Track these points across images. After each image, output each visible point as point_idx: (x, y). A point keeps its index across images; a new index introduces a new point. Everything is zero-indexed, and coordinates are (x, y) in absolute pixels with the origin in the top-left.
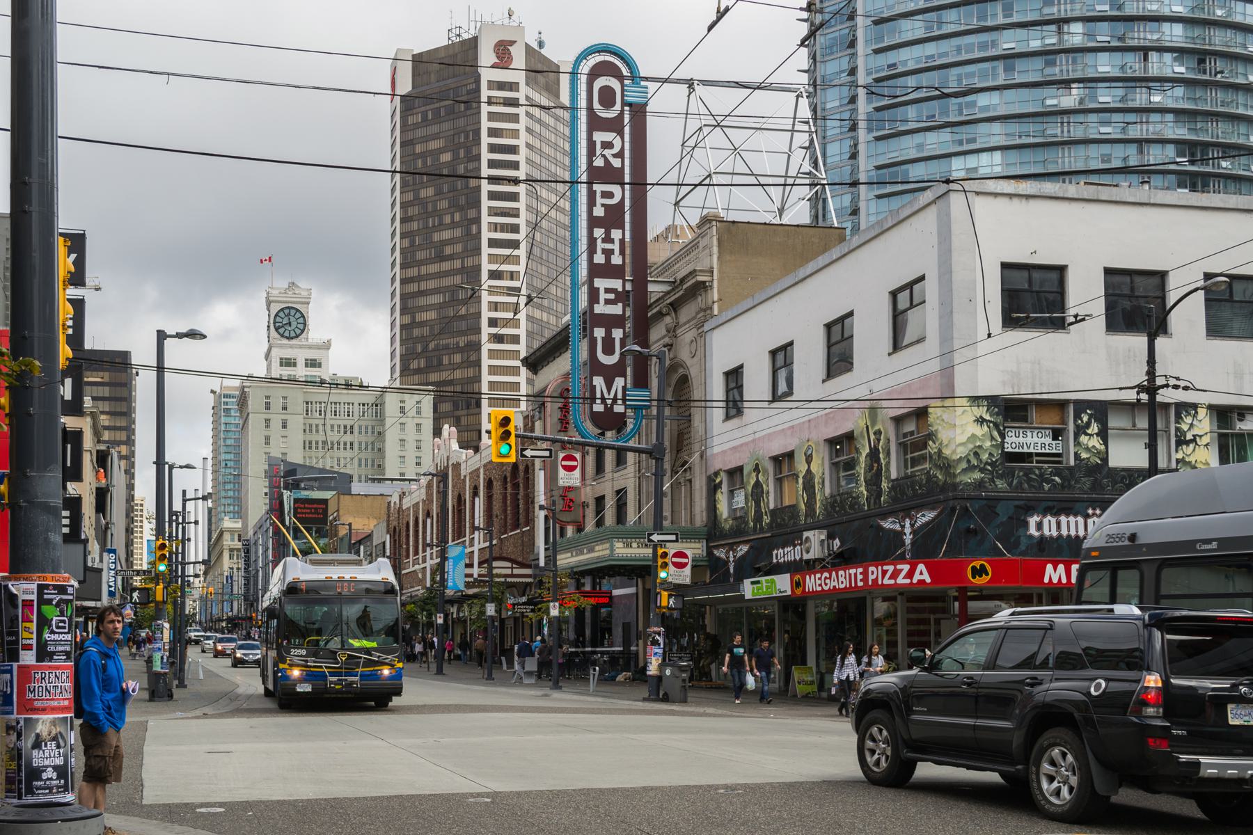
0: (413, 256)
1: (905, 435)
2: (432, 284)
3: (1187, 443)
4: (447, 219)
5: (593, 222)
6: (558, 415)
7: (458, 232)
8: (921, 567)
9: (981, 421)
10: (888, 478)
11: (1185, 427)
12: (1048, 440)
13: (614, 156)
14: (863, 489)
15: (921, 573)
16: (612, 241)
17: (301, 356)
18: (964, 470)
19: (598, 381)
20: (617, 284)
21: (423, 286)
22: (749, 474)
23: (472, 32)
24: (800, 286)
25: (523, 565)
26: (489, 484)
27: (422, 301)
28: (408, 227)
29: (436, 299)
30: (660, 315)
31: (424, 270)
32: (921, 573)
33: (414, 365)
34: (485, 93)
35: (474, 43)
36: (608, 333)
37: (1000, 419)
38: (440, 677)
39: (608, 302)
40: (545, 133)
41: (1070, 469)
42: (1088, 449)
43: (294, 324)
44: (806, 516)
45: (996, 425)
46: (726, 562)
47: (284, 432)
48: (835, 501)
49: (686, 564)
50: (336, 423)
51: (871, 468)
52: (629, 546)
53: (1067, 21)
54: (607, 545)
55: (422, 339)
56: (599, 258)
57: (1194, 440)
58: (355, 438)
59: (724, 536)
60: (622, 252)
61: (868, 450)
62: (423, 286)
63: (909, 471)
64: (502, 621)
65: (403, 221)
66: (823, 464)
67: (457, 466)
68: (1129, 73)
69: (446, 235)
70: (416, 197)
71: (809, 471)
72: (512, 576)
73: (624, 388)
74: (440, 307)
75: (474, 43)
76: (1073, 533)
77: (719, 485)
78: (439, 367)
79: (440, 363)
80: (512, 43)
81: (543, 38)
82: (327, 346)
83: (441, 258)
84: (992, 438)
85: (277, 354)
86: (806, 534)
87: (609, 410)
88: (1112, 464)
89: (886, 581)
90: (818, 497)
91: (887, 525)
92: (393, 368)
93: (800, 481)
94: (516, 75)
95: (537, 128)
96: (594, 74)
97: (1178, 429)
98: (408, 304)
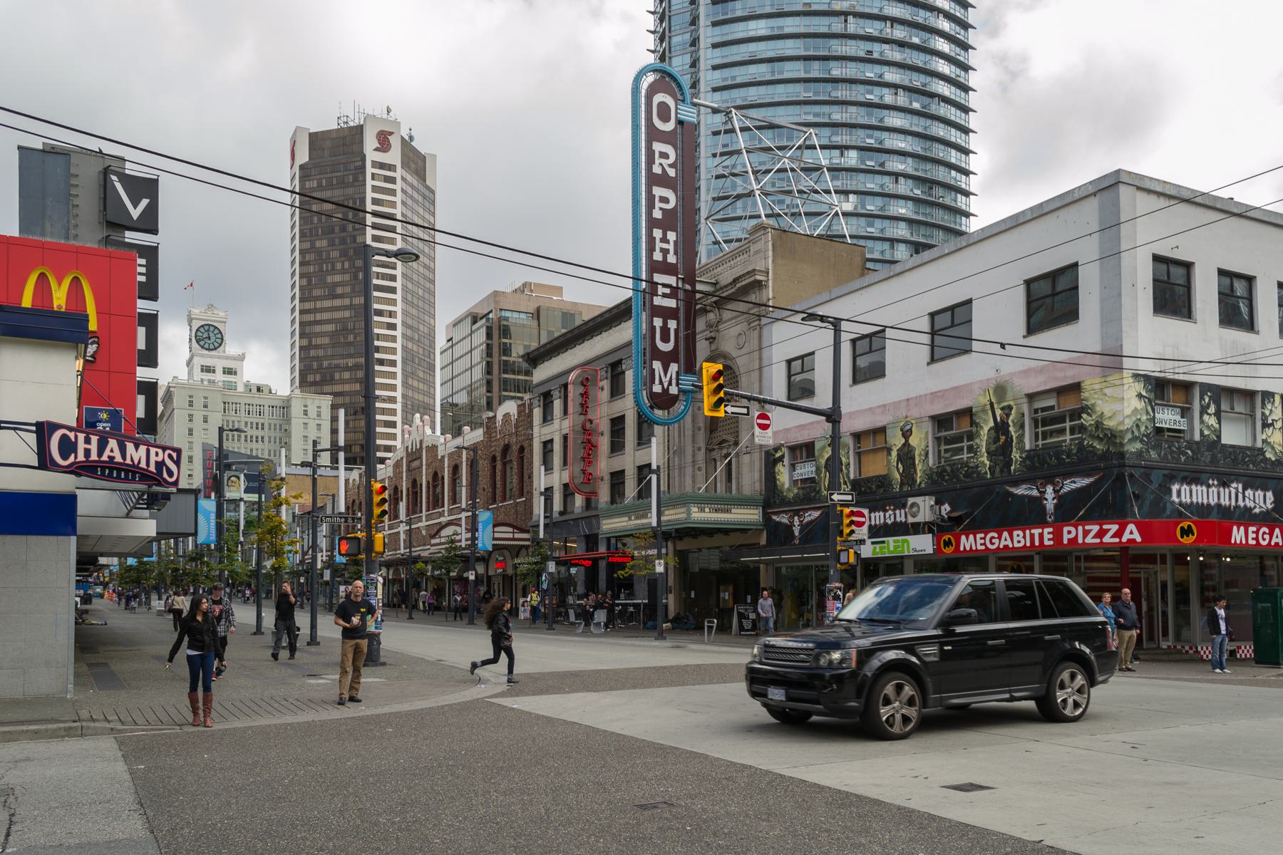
0: (310, 292)
1: (1036, 411)
2: (326, 316)
3: (1269, 426)
4: (339, 266)
5: (652, 224)
6: (580, 400)
7: (347, 277)
8: (1131, 527)
9: (1140, 396)
10: (1022, 449)
11: (1267, 413)
12: (1178, 418)
13: (670, 166)
14: (985, 459)
15: (1131, 533)
16: (668, 242)
17: (219, 365)
18: (1130, 440)
19: (657, 365)
20: (671, 280)
21: (318, 317)
22: (823, 448)
23: (357, 122)
24: (894, 280)
25: (522, 531)
26: (472, 464)
27: (318, 329)
28: (305, 269)
29: (329, 328)
30: (704, 311)
31: (319, 304)
32: (1131, 533)
33: (311, 378)
34: (369, 170)
35: (359, 129)
36: (665, 323)
37: (1152, 396)
38: (724, 637)
39: (664, 295)
40: (415, 207)
41: (1197, 443)
42: (1208, 427)
43: (213, 339)
44: (902, 484)
45: (1150, 401)
46: (789, 527)
47: (205, 426)
48: (945, 471)
49: (863, 523)
50: (249, 420)
51: (997, 440)
52: (702, 510)
53: (848, 148)
54: (683, 510)
55: (318, 358)
56: (658, 256)
57: (1272, 424)
58: (266, 433)
59: (784, 502)
60: (676, 253)
61: (992, 424)
62: (318, 317)
63: (1040, 442)
64: (489, 578)
65: (301, 264)
66: (927, 438)
67: (433, 449)
68: (886, 191)
69: (338, 278)
70: (313, 246)
71: (906, 444)
72: (514, 539)
73: (678, 373)
74: (332, 335)
75: (359, 129)
76: (1205, 501)
77: (781, 459)
78: (331, 381)
79: (332, 379)
80: (391, 133)
81: (413, 133)
82: (241, 358)
83: (335, 297)
84: (1148, 413)
85: (198, 361)
86: (911, 500)
87: (666, 391)
88: (1224, 441)
89: (1089, 540)
90: (919, 468)
91: (1020, 491)
92: (292, 380)
93: (894, 454)
94: (394, 156)
95: (409, 202)
96: (652, 91)
97: (1263, 414)
98: (306, 330)
